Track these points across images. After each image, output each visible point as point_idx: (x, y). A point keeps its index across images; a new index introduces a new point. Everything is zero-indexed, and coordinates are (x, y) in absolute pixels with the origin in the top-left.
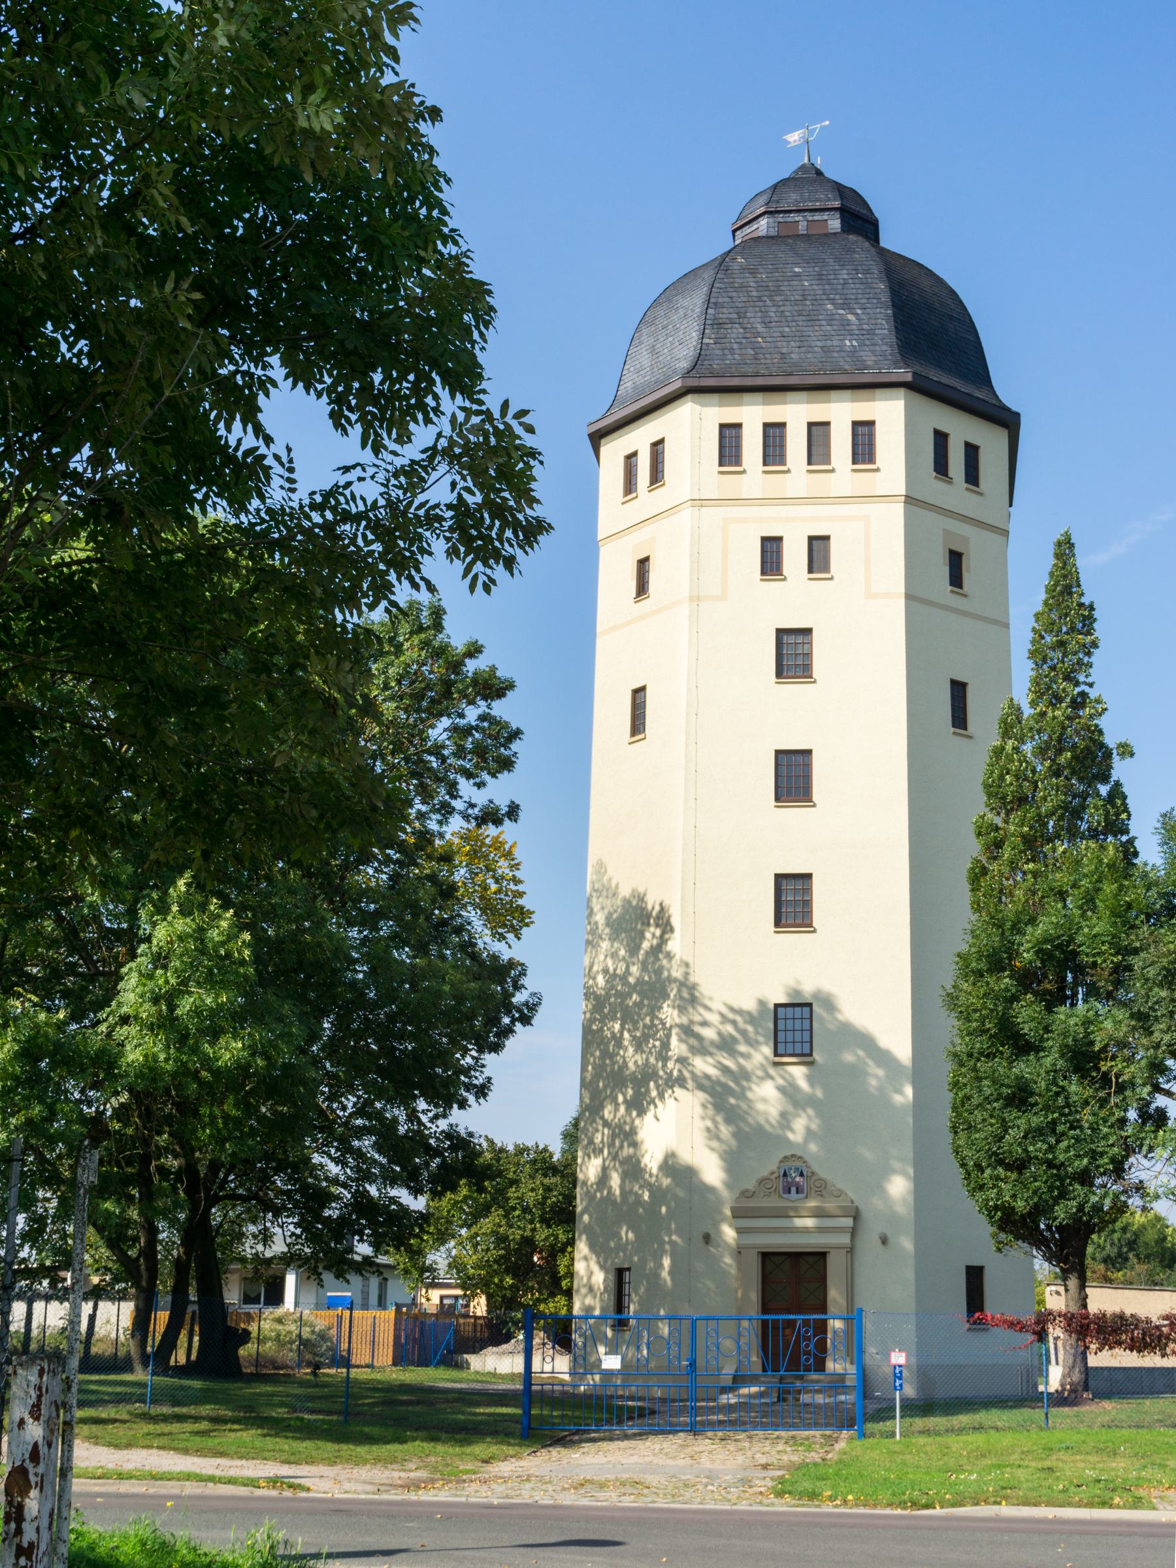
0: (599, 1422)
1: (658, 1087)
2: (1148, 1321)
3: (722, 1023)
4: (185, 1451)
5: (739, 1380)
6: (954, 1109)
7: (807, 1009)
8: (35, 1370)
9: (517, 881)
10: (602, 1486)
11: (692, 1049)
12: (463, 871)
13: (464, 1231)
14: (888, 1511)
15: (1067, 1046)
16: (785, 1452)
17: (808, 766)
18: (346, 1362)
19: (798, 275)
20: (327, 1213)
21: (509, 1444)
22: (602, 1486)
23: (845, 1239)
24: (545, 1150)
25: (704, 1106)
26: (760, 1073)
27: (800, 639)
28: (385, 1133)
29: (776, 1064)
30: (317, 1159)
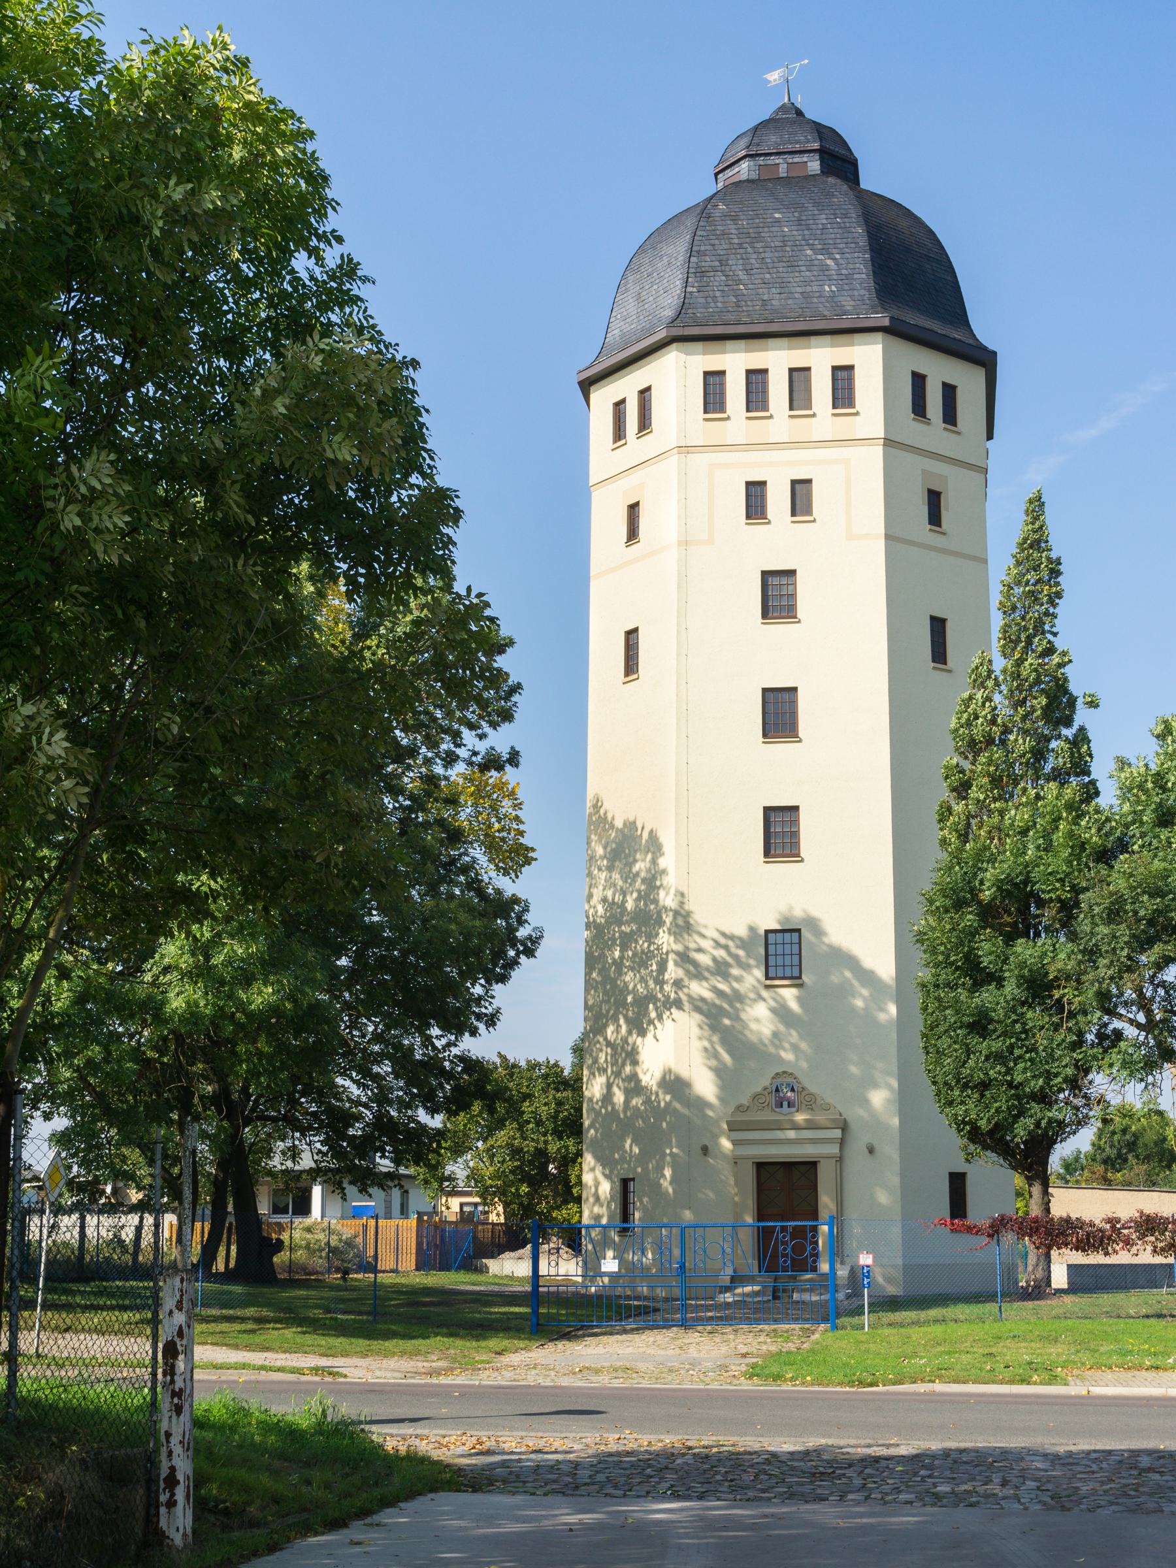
0: (600, 1319)
1: (656, 1009)
2: (1092, 1224)
3: (714, 948)
4: (236, 1347)
5: (737, 1280)
6: (924, 1035)
7: (796, 935)
8: (178, 1279)
9: (517, 819)
10: (597, 1371)
11: (687, 972)
12: (468, 811)
13: (480, 1144)
14: (838, 1389)
15: (1023, 977)
16: (765, 1343)
17: (794, 703)
18: (375, 1271)
19: (778, 221)
20: (351, 1132)
21: (519, 1338)
22: (597, 1371)
23: (834, 1149)
24: (556, 1065)
25: (700, 1027)
26: (752, 995)
27: (784, 581)
28: (403, 1061)
29: (767, 987)
30: (339, 1081)
